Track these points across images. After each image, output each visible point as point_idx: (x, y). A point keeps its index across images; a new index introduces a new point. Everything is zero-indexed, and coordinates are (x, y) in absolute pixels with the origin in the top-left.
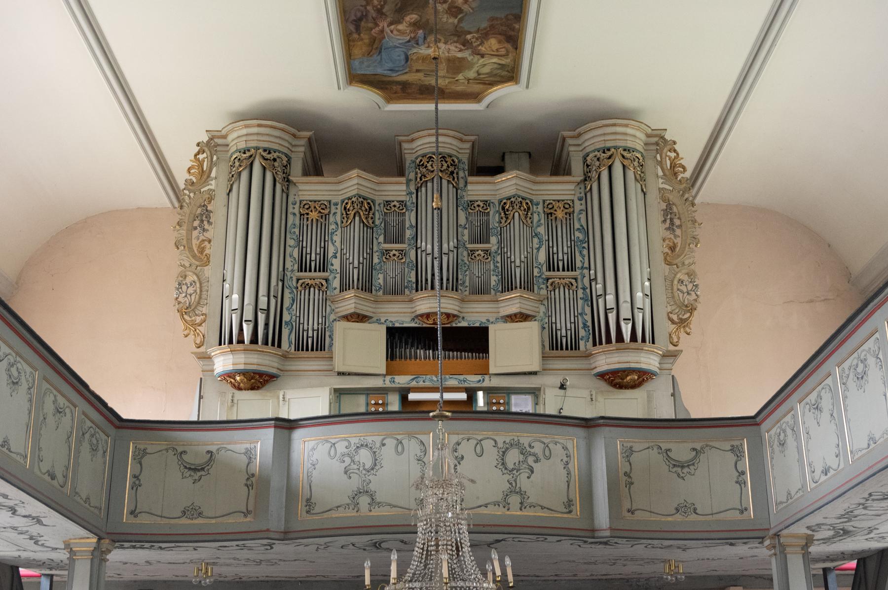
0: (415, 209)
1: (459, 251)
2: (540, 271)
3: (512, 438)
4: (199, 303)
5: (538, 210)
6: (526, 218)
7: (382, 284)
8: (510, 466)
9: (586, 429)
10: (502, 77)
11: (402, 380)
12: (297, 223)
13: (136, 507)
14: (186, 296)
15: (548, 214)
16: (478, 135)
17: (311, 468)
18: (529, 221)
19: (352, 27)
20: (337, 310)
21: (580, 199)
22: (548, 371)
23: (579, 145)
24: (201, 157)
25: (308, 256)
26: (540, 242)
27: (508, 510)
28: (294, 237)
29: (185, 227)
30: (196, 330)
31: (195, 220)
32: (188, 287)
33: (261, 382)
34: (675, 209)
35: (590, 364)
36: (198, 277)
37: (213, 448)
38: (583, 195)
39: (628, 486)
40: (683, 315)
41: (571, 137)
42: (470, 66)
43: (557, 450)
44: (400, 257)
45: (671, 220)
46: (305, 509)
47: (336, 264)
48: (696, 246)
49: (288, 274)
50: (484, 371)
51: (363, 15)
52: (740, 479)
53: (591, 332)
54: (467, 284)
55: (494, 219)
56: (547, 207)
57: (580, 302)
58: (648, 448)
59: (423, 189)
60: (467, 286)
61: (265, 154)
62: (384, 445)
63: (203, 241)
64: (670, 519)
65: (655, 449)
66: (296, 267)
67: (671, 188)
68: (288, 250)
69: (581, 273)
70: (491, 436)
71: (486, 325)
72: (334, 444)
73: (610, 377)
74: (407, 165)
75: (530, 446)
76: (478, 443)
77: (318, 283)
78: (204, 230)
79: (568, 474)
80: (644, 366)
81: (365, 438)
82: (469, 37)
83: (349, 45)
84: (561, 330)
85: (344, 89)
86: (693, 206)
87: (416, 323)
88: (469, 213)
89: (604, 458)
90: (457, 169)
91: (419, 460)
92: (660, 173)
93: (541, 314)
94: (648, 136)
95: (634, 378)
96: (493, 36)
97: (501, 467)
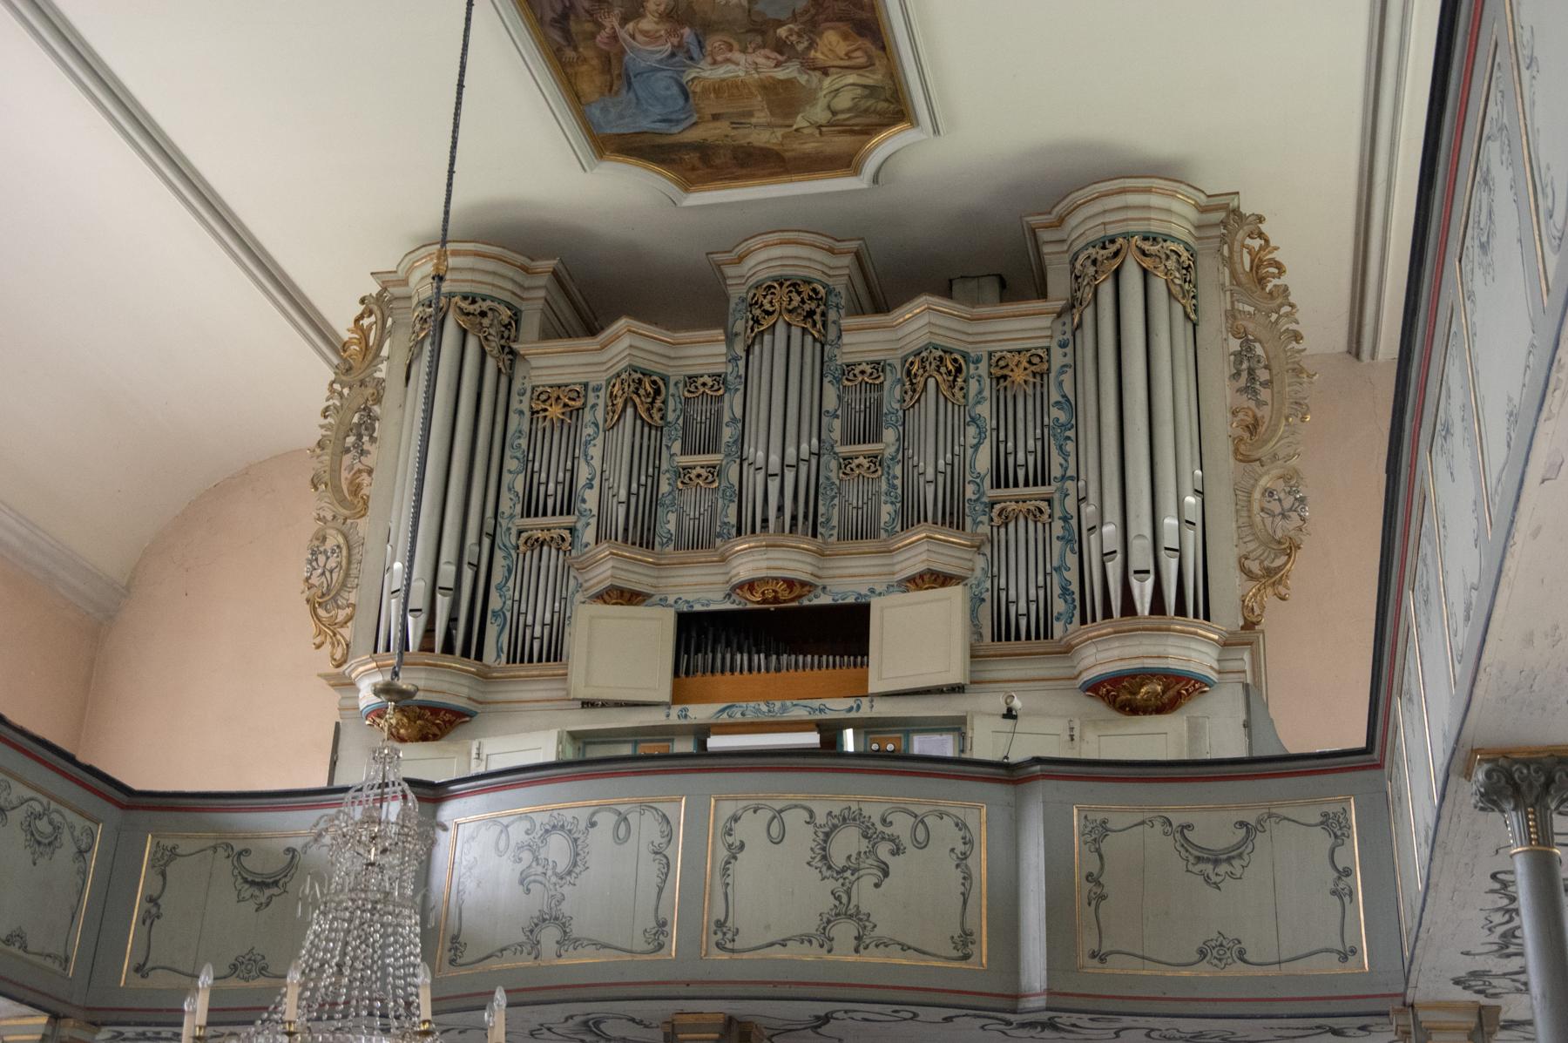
0: (742, 387)
1: (822, 460)
2: (979, 491)
3: (845, 805)
4: (344, 585)
5: (979, 372)
6: (952, 386)
7: (673, 532)
8: (839, 861)
9: (1010, 788)
10: (880, 114)
11: (700, 713)
12: (526, 428)
13: (147, 958)
14: (323, 574)
15: (998, 379)
16: (862, 239)
17: (464, 874)
18: (959, 395)
19: (556, 36)
20: (586, 585)
21: (1063, 345)
22: (987, 685)
23: (1063, 241)
24: (366, 322)
25: (542, 488)
26: (980, 433)
27: (830, 951)
28: (519, 454)
29: (328, 451)
30: (335, 635)
31: (348, 436)
32: (328, 558)
33: (437, 725)
34: (1259, 350)
36: (346, 538)
37: (296, 843)
38: (1068, 336)
39: (1094, 903)
41: (1046, 228)
42: (810, 97)
43: (944, 831)
44: (710, 479)
45: (1251, 371)
46: (448, 955)
47: (591, 498)
48: (1303, 419)
49: (504, 522)
50: (860, 690)
51: (565, 6)
52: (1341, 886)
53: (1077, 603)
54: (835, 522)
55: (892, 396)
56: (997, 365)
57: (1057, 545)
58: (1143, 823)
59: (757, 348)
60: (834, 527)
61: (464, 305)
62: (593, 825)
63: (360, 471)
64: (1185, 973)
65: (1158, 826)
66: (518, 508)
67: (1251, 309)
68: (506, 478)
70: (803, 803)
72: (507, 826)
74: (732, 305)
75: (884, 821)
76: (774, 817)
77: (555, 536)
78: (363, 453)
79: (964, 878)
80: (1173, 664)
81: (561, 812)
82: (782, 32)
83: (566, 74)
84: (1017, 602)
85: (592, 170)
87: (734, 602)
88: (844, 387)
89: (1042, 843)
90: (822, 307)
91: (656, 853)
93: (978, 573)
94: (1203, 210)
95: (1155, 691)
96: (828, 24)
97: (820, 864)
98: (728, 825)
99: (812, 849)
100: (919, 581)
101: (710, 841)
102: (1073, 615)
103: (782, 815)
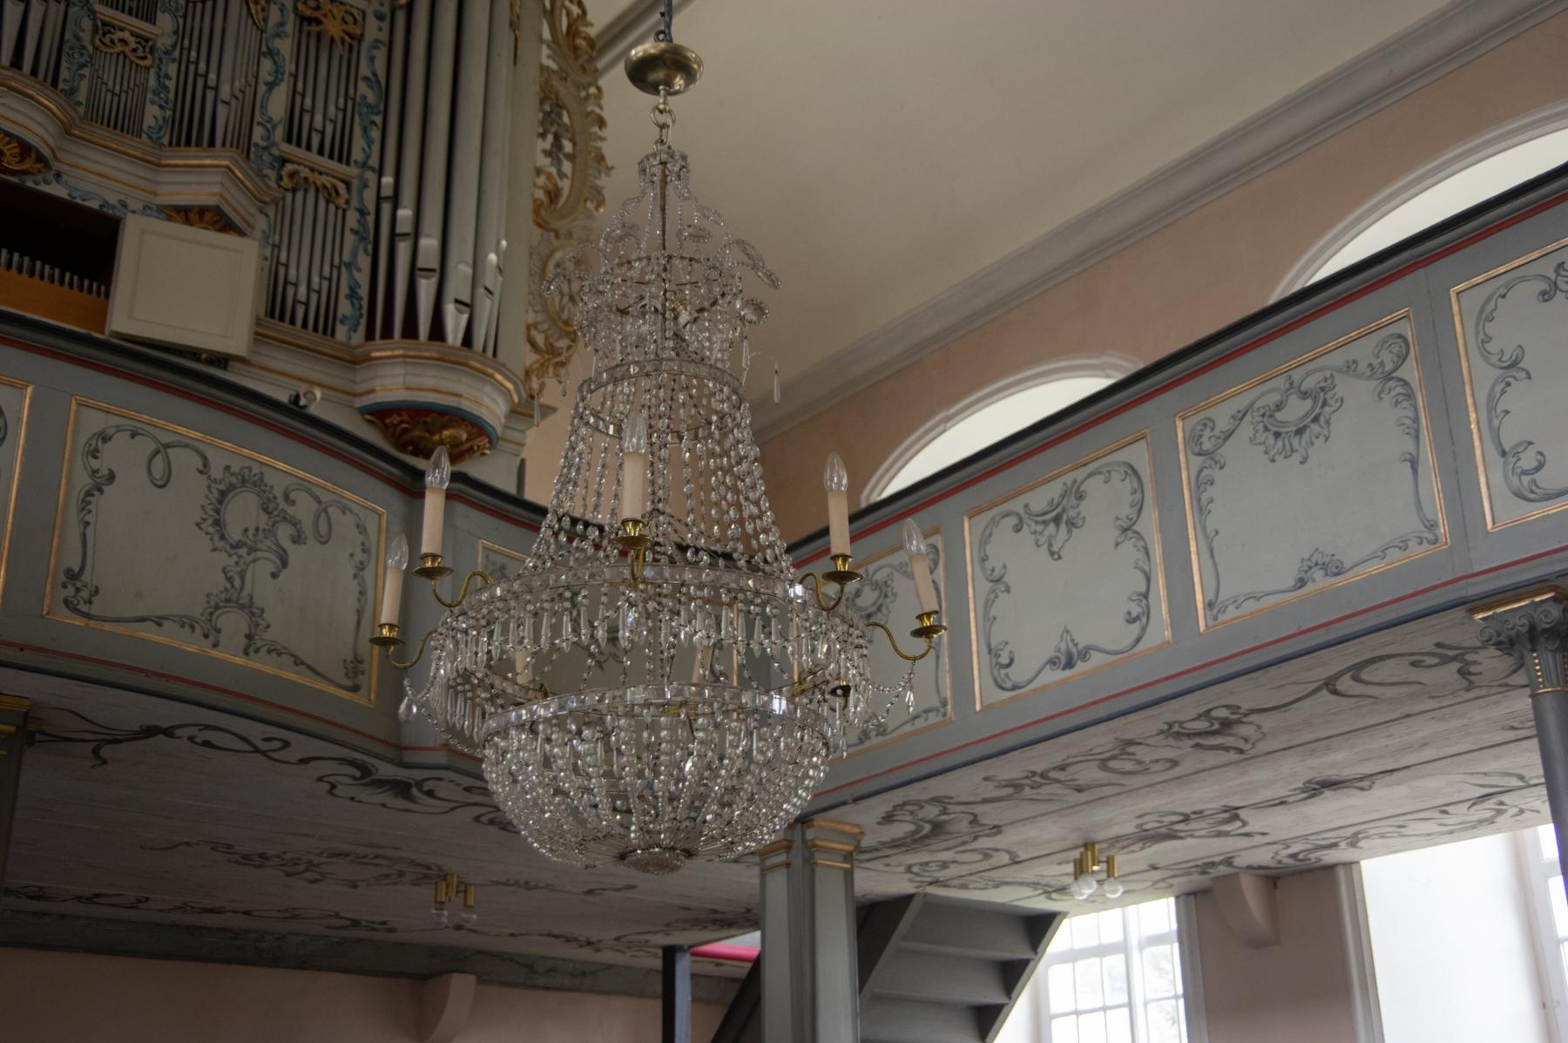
2: (269, 133)
8: (235, 534)
21: (380, 17)
26: (276, 72)
27: (215, 645)
35: (354, 382)
40: (558, 340)
45: (557, 138)
48: (597, 208)
53: (365, 311)
54: (82, 96)
57: (350, 239)
60: (79, 103)
69: (361, 177)
71: (117, 213)
73: (401, 422)
75: (287, 497)
76: (157, 452)
84: (296, 285)
86: (600, 128)
92: (547, 34)
97: (211, 530)
98: (94, 442)
99: (203, 507)
100: (193, 216)
101: (67, 456)
102: (359, 324)
103: (170, 451)
